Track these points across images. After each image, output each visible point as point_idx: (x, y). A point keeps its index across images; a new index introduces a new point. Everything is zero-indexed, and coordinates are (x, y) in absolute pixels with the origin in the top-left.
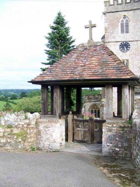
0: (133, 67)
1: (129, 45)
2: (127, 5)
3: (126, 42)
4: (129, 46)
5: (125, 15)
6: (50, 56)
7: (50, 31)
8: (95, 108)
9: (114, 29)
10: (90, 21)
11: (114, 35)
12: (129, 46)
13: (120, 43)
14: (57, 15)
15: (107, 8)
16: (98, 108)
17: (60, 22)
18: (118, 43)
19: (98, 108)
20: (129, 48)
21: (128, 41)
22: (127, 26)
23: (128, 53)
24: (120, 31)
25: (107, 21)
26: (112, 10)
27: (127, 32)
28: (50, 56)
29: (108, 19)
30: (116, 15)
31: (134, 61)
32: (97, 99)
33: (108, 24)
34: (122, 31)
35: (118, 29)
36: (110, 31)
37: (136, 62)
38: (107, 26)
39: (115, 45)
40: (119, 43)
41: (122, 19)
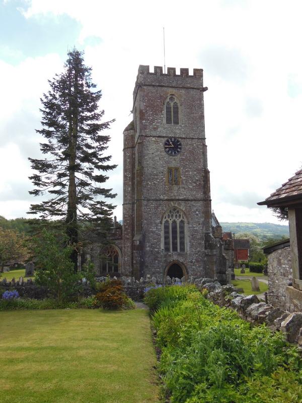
0: (186, 182)
1: (180, 145)
2: (176, 78)
3: (175, 138)
4: (179, 147)
5: (173, 95)
6: (48, 110)
7: (68, 57)
8: (109, 252)
9: (157, 114)
10: (111, 156)
11: (155, 125)
12: (179, 147)
13: (166, 139)
14: (61, 69)
15: (144, 78)
16: (115, 252)
17: (76, 63)
18: (162, 139)
19: (115, 252)
20: (180, 148)
21: (179, 138)
22: (176, 112)
23: (178, 157)
24: (165, 121)
25: (143, 99)
26: (152, 82)
27: (176, 123)
28: (48, 110)
29: (146, 96)
30: (158, 92)
31: (187, 171)
32: (114, 236)
33: (145, 104)
34: (169, 121)
35: (162, 116)
36: (149, 118)
37: (190, 173)
38: (143, 108)
39: (156, 142)
40: (164, 140)
41: (168, 100)
